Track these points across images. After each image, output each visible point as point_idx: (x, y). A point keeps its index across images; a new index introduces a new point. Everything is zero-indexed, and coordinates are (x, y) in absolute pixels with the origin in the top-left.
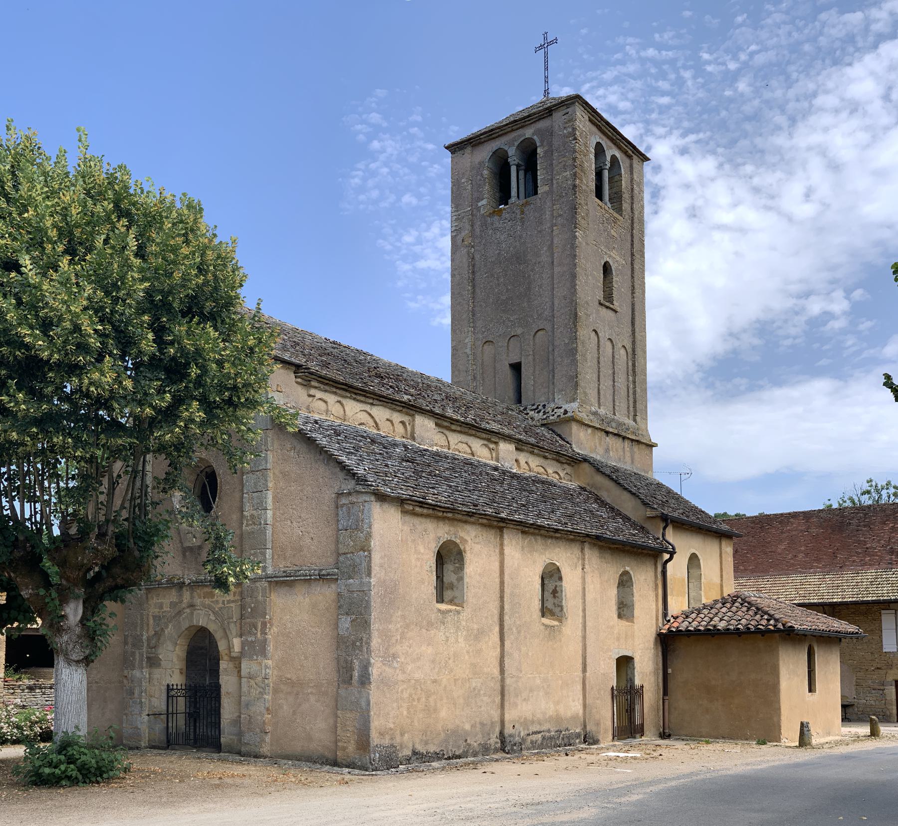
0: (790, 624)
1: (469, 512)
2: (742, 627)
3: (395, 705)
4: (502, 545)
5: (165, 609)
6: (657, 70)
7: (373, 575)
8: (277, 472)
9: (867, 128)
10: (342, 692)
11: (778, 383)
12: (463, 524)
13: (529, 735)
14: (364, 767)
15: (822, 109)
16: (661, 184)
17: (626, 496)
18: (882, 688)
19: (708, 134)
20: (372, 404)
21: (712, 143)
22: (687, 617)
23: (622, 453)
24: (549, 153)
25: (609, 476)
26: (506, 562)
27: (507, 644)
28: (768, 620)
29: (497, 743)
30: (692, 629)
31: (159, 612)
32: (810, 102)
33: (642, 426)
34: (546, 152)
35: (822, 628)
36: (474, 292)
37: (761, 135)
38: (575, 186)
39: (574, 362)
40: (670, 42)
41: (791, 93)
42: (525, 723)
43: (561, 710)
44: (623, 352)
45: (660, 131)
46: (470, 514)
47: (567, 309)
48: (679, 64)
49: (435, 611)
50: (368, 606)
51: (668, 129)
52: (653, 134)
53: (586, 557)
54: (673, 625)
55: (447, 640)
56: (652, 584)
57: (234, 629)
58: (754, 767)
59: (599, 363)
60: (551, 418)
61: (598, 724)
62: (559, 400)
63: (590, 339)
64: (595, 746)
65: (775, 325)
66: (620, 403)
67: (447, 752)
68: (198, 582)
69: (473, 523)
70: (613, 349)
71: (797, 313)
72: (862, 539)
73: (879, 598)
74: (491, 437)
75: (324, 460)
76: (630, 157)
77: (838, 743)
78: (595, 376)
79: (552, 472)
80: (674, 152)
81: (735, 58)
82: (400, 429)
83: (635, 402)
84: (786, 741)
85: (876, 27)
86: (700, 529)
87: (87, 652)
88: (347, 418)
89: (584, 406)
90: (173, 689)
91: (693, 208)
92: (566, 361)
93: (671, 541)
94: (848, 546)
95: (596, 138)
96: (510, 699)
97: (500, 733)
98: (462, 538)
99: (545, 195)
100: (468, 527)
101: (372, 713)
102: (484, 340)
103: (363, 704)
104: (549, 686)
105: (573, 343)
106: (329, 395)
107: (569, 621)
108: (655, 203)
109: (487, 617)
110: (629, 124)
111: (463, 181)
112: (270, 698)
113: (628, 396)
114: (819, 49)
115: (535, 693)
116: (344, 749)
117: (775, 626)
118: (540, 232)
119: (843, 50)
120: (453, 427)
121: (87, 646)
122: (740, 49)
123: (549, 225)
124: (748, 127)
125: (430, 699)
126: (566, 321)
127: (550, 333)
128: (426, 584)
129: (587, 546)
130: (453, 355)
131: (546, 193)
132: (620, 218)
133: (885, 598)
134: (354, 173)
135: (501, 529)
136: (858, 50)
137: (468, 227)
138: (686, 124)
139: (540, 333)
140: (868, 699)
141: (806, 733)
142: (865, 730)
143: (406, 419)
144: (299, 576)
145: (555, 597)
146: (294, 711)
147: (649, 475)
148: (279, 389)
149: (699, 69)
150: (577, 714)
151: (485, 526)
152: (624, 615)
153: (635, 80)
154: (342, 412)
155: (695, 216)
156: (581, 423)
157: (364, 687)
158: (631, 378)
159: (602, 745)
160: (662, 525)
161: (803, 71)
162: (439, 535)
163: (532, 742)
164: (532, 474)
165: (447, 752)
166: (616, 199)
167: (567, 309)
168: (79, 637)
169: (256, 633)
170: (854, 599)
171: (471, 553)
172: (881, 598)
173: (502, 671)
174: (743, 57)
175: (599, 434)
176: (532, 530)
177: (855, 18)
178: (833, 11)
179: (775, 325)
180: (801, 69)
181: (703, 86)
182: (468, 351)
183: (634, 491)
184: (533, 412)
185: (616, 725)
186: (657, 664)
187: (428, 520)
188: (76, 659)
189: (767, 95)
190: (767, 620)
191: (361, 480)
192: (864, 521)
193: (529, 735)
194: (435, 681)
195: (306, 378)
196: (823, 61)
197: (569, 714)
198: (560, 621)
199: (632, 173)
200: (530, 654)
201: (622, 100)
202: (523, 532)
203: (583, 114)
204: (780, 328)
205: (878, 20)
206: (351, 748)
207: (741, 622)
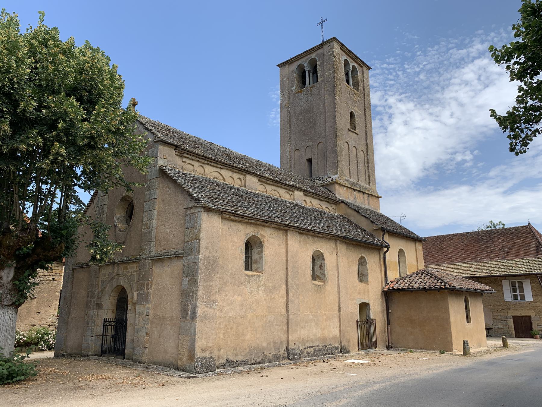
0: (453, 285)
1: (265, 220)
2: (427, 287)
3: (214, 332)
4: (287, 239)
5: (106, 277)
6: (388, 72)
7: (200, 253)
8: (160, 200)
9: (472, 91)
10: (182, 323)
11: (446, 188)
12: (262, 227)
13: (305, 348)
14: (191, 371)
15: (454, 84)
16: (392, 113)
17: (363, 219)
18: (506, 320)
19: (410, 94)
20: (221, 168)
21: (412, 97)
22: (398, 282)
23: (363, 200)
24: (322, 64)
25: (354, 209)
26: (289, 249)
27: (290, 295)
28: (441, 283)
29: (284, 354)
30: (400, 288)
31: (104, 278)
32: (449, 82)
33: (373, 187)
34: (321, 63)
35: (471, 287)
36: (290, 128)
37: (431, 94)
38: (334, 76)
39: (336, 156)
40: (392, 62)
41: (441, 79)
42: (303, 342)
43: (326, 333)
44: (362, 153)
45: (391, 93)
46: (266, 221)
47: (332, 132)
48: (397, 69)
49: (244, 275)
50: (197, 272)
51: (394, 93)
52: (388, 95)
53: (338, 248)
54: (390, 286)
55: (252, 293)
56: (378, 264)
57: (135, 287)
58: (434, 372)
59: (349, 157)
60: (326, 182)
61: (349, 342)
62: (329, 174)
63: (344, 145)
64: (347, 355)
65: (443, 165)
66: (361, 176)
67: (251, 360)
68: (121, 261)
69: (269, 227)
70: (357, 151)
71: (452, 160)
72: (489, 246)
73: (500, 274)
74: (290, 188)
75: (181, 191)
76: (362, 67)
77: (486, 352)
78: (348, 163)
79: (324, 207)
80: (397, 101)
81: (418, 66)
82: (239, 182)
83: (369, 176)
84: (456, 351)
85: (472, 55)
86: (404, 236)
87: (14, 300)
88: (206, 174)
89: (342, 176)
90: (106, 321)
91: (406, 121)
92: (332, 156)
93: (388, 242)
94: (483, 249)
95: (344, 57)
96: (292, 327)
97: (287, 348)
98: (261, 235)
99: (321, 82)
100: (266, 229)
101: (197, 337)
102: (295, 149)
103: (193, 331)
104: (318, 320)
105: (335, 147)
106: (195, 162)
107: (329, 282)
108: (390, 120)
109: (277, 280)
110: (378, 91)
111: (285, 79)
112: (149, 327)
113: (365, 174)
114: (451, 63)
115: (309, 324)
116: (182, 359)
117: (445, 286)
118: (319, 98)
119: (460, 63)
120: (268, 182)
121: (15, 296)
122: (420, 63)
123: (323, 95)
124: (425, 91)
125: (239, 328)
126: (332, 137)
127: (325, 144)
128: (238, 260)
129: (338, 242)
130: (281, 157)
131: (322, 81)
132: (358, 93)
133: (503, 274)
134: (272, 113)
135: (286, 231)
136: (466, 63)
137: (287, 99)
138: (401, 91)
139: (320, 144)
140: (499, 325)
141: (466, 347)
142: (499, 343)
143: (241, 177)
144: (166, 256)
145: (321, 269)
146: (160, 335)
147: (378, 211)
148: (165, 157)
149: (404, 71)
150: (336, 336)
151: (277, 229)
152: (363, 281)
153: (380, 75)
154: (203, 171)
155: (407, 124)
156: (340, 185)
157: (193, 321)
158: (366, 165)
159: (351, 354)
160: (382, 233)
161: (445, 71)
162: (247, 232)
163: (307, 353)
164: (314, 207)
165: (251, 360)
166: (356, 85)
167: (332, 132)
168: (10, 291)
169: (144, 289)
170: (488, 275)
171: (268, 243)
172: (501, 274)
173: (287, 311)
174: (421, 66)
175: (351, 191)
176: (305, 232)
177: (463, 52)
178: (455, 49)
179: (443, 165)
180: (444, 70)
181: (406, 77)
182: (288, 155)
183: (367, 216)
184: (317, 181)
185: (360, 342)
186: (383, 307)
187: (240, 224)
188: (7, 304)
189: (432, 79)
190: (440, 282)
191: (197, 200)
192: (489, 237)
193: (305, 348)
194: (243, 317)
195: (180, 152)
196: (453, 67)
197: (331, 336)
198: (324, 283)
199: (363, 74)
200: (306, 301)
201: (375, 83)
202: (300, 233)
203: (338, 46)
204: (445, 166)
205: (472, 52)
206: (185, 358)
207: (426, 284)
